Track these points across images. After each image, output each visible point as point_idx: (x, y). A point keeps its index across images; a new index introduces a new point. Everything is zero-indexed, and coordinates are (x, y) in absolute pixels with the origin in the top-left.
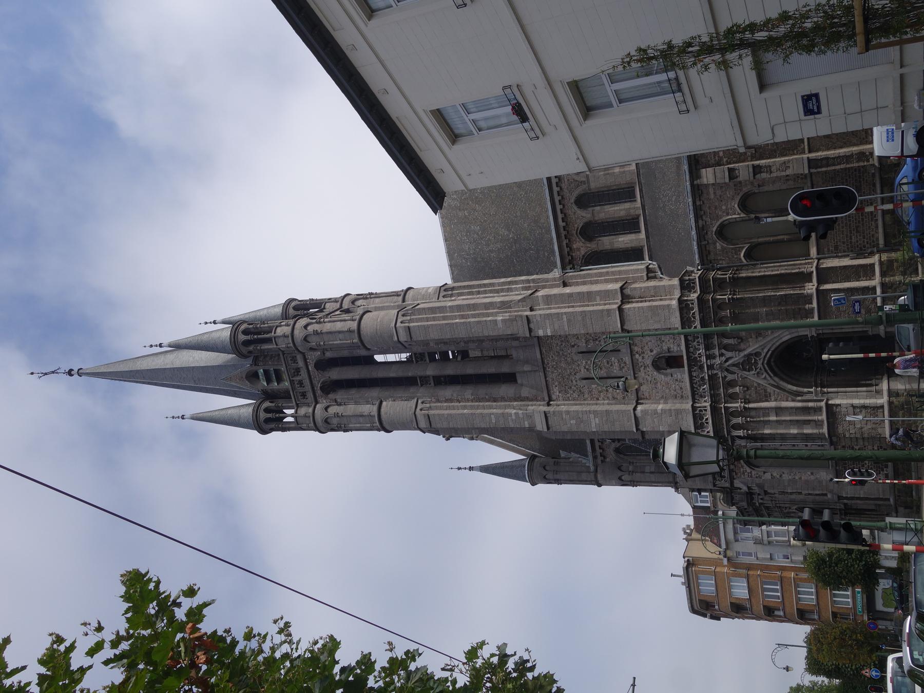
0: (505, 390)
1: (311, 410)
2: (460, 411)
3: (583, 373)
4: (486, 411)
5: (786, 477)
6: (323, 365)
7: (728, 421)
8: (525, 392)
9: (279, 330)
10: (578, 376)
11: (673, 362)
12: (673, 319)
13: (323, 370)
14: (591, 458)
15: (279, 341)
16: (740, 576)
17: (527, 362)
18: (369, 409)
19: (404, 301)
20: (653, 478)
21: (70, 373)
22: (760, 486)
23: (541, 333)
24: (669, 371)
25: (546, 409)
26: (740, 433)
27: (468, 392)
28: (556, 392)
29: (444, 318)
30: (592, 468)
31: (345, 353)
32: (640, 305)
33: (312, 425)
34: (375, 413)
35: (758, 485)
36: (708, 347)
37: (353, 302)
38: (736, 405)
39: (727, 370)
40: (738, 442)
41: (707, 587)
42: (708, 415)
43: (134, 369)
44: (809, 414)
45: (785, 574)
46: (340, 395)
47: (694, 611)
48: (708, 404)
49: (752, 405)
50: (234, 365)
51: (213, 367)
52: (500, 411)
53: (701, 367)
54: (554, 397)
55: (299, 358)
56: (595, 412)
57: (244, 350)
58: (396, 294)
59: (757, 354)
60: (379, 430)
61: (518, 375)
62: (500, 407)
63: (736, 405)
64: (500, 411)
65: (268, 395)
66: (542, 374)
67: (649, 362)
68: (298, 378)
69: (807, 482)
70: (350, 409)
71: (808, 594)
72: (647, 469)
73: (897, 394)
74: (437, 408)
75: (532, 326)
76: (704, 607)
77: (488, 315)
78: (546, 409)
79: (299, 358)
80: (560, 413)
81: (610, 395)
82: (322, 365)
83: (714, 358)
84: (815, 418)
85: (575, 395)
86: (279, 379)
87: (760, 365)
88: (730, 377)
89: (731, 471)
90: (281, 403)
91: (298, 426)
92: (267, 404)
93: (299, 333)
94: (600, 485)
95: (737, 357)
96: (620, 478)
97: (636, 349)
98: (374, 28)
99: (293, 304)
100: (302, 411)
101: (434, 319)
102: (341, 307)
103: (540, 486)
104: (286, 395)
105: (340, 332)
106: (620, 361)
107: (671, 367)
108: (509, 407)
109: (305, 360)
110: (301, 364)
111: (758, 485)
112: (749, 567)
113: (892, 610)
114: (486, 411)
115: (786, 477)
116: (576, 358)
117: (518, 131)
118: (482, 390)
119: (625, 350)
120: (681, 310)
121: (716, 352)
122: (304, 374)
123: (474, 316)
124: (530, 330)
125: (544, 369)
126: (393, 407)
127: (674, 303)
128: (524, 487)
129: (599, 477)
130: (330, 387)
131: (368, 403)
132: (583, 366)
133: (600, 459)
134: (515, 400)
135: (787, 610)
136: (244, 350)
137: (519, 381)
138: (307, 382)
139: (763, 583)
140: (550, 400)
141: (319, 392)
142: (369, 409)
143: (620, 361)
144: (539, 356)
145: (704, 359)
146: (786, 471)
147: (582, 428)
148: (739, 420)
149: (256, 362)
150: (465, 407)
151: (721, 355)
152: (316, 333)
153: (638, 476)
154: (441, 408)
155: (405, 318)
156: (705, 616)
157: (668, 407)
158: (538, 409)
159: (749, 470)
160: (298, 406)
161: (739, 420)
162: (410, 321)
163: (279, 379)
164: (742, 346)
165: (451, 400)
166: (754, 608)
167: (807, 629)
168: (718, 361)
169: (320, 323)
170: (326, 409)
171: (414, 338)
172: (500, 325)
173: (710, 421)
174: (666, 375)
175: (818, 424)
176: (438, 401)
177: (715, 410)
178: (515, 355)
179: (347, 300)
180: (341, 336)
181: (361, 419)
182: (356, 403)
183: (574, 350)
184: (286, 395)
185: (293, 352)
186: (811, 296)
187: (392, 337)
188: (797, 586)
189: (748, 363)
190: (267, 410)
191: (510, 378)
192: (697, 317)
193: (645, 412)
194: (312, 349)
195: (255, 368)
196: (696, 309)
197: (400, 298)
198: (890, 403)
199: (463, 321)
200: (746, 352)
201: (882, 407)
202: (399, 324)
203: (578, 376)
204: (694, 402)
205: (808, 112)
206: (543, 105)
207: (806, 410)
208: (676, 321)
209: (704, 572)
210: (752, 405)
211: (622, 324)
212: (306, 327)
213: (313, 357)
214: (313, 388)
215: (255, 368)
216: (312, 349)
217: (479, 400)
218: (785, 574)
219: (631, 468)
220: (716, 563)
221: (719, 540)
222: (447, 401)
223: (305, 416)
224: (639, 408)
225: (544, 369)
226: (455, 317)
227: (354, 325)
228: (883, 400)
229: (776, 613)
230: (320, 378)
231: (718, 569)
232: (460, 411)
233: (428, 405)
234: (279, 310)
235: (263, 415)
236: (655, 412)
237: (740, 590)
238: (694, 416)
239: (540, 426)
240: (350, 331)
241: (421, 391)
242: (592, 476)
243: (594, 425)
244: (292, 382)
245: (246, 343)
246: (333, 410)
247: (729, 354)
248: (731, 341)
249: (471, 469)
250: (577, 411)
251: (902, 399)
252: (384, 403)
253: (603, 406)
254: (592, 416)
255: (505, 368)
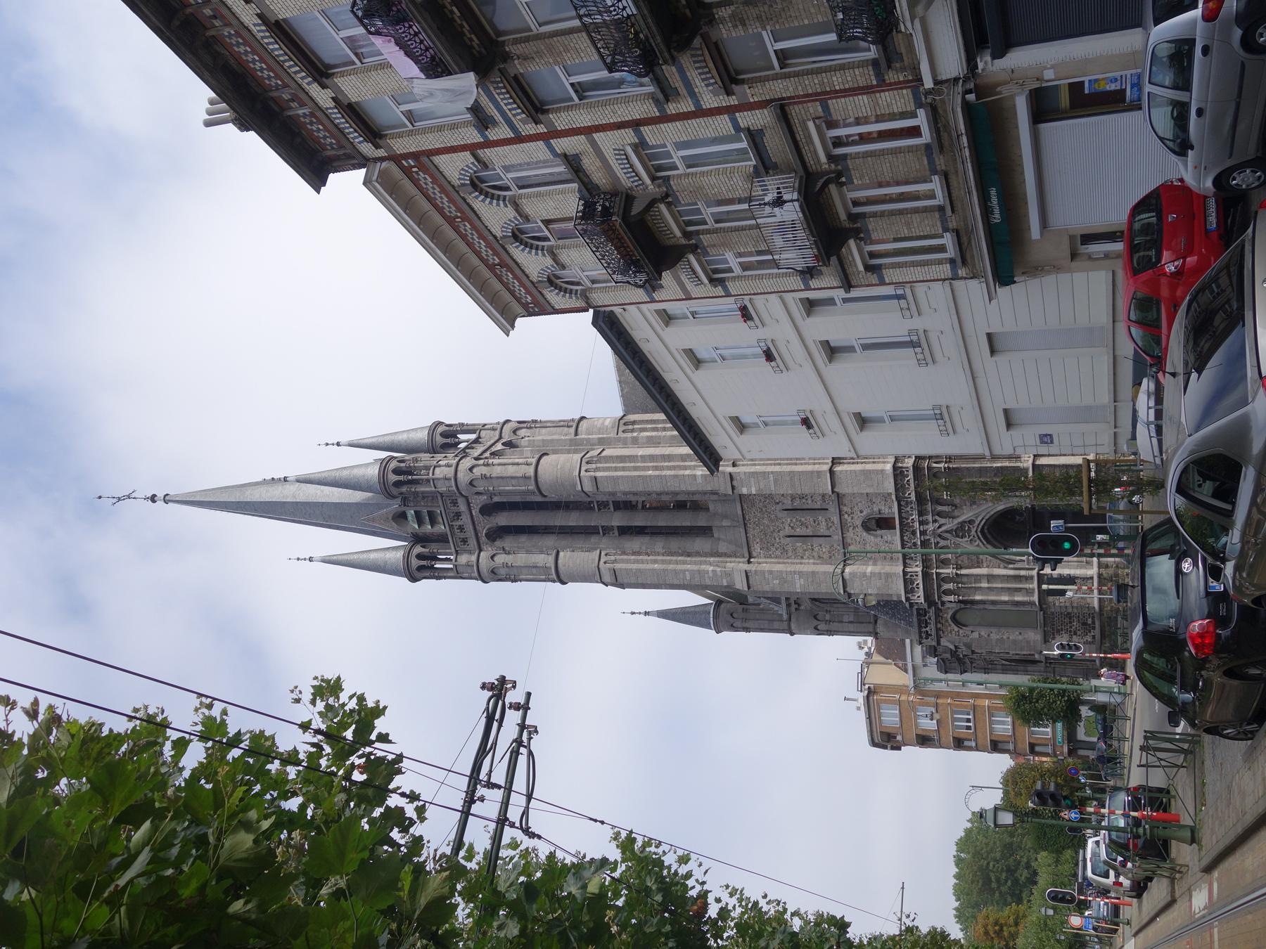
0: (699, 544)
1: (474, 558)
2: (650, 566)
3: (788, 531)
4: (680, 567)
5: (994, 636)
6: (490, 509)
7: (939, 586)
8: (723, 547)
9: (437, 470)
10: (782, 534)
11: (883, 523)
12: (886, 484)
13: (489, 515)
14: (784, 605)
15: (439, 484)
16: (928, 704)
17: (726, 517)
18: (546, 560)
19: (576, 434)
20: (851, 627)
21: (153, 499)
22: (968, 646)
23: (745, 491)
24: (879, 532)
25: (746, 567)
26: (952, 598)
27: (659, 544)
28: (757, 549)
29: (636, 469)
30: (785, 617)
31: (518, 499)
32: (853, 467)
33: (476, 574)
34: (551, 564)
35: (965, 645)
36: (921, 514)
37: (514, 432)
38: (948, 571)
39: (940, 536)
40: (948, 605)
41: (890, 717)
42: (920, 581)
43: (242, 499)
44: (1021, 582)
45: (979, 702)
46: (508, 542)
47: (874, 744)
48: (919, 569)
49: (964, 572)
50: (377, 504)
51: (349, 504)
52: (695, 567)
53: (914, 533)
54: (754, 554)
55: (461, 501)
56: (800, 573)
57: (395, 491)
58: (566, 424)
59: (971, 522)
60: (554, 581)
61: (715, 530)
62: (695, 563)
63: (948, 571)
64: (695, 567)
65: (418, 539)
66: (742, 530)
67: (859, 523)
68: (459, 523)
69: (1015, 642)
70: (520, 559)
71: (1004, 725)
72: (846, 618)
73: (1107, 566)
74: (623, 561)
75: (735, 483)
76: (885, 739)
77: (685, 468)
78: (746, 567)
79: (461, 501)
80: (763, 572)
81: (815, 554)
82: (488, 510)
83: (927, 524)
84: (1027, 586)
85: (778, 553)
86: (433, 522)
87: (973, 532)
88: (942, 543)
89: (938, 630)
90: (434, 547)
91: (458, 574)
92: (418, 549)
93: (464, 477)
94: (792, 634)
95: (950, 524)
96: (816, 628)
97: (845, 509)
98: (700, 376)
99: (441, 429)
100: (463, 559)
101: (624, 469)
102: (501, 438)
103: (727, 635)
104: (442, 539)
105: (512, 478)
106: (828, 520)
107: (881, 528)
108: (706, 563)
109: (469, 504)
110: (462, 507)
111: (965, 645)
112: (938, 695)
113: (1095, 740)
114: (680, 567)
115: (994, 636)
116: (780, 515)
117: (767, 367)
118: (675, 543)
119: (833, 509)
120: (895, 476)
121: (930, 518)
122: (465, 519)
123: (669, 468)
124: (733, 488)
125: (745, 525)
126: (570, 558)
127: (889, 467)
128: (706, 636)
129: (793, 626)
130: (496, 534)
131: (542, 552)
132: (787, 524)
133: (794, 606)
134: (712, 555)
135: (980, 742)
136: (395, 491)
137: (716, 535)
138: (469, 528)
139: (953, 712)
140: (750, 557)
141: (483, 539)
142: (546, 560)
143: (828, 520)
144: (740, 512)
145: (917, 525)
146: (994, 630)
147: (786, 588)
148: (951, 586)
149: (405, 501)
150: (655, 562)
151: (935, 521)
152: (484, 477)
153: (834, 626)
154: (628, 561)
155: (589, 466)
156: (885, 747)
157: (877, 569)
158: (737, 566)
159: (956, 629)
160: (457, 552)
161: (951, 586)
162: (597, 470)
163: (433, 522)
164: (956, 513)
165: (639, 553)
166: (943, 739)
167: (1004, 762)
168: (931, 527)
169: (488, 465)
170: (492, 557)
171: (601, 489)
172: (699, 480)
173: (921, 586)
174: (876, 536)
175: (1029, 592)
176: (624, 553)
177: (926, 575)
178: (711, 507)
179: (507, 428)
180: (514, 482)
181: (534, 571)
182: (528, 552)
183: (779, 507)
184: (442, 539)
185: (453, 496)
186: (1027, 469)
187: (574, 485)
188: (991, 715)
189: (961, 531)
190: (419, 557)
191: (705, 531)
192: (912, 485)
193: (853, 574)
194: (477, 493)
195: (403, 508)
196: (911, 476)
197: (572, 430)
198: (1100, 576)
199: (657, 473)
200: (960, 520)
201: (1092, 578)
202: (583, 473)
203: (782, 534)
204: (905, 567)
205: (1042, 442)
206: (828, 421)
207: (1017, 578)
208: (890, 487)
209: (886, 702)
210: (964, 572)
211: (833, 486)
212: (471, 469)
213: (478, 502)
214: (476, 535)
215: (403, 508)
216: (477, 493)
217: (671, 554)
218: (979, 702)
219: (828, 617)
220: (901, 689)
221: (904, 659)
222: (634, 553)
223: (468, 565)
224: (847, 570)
225: (745, 525)
226: (648, 468)
227: (530, 471)
228: (1093, 571)
229: (966, 743)
230: (485, 524)
231: (904, 698)
232: (650, 566)
233: (613, 558)
234: (423, 436)
235: (415, 563)
236: (864, 574)
237: (928, 725)
238: (905, 580)
239: (740, 585)
240: (525, 478)
241: (605, 541)
242: (785, 625)
243: (798, 586)
244: (451, 527)
245: (398, 484)
246: (501, 559)
247: (942, 521)
248: (945, 508)
249: (646, 613)
250: (781, 572)
251: (1111, 571)
252: (561, 554)
253: (808, 566)
254: (797, 577)
255: (701, 521)
